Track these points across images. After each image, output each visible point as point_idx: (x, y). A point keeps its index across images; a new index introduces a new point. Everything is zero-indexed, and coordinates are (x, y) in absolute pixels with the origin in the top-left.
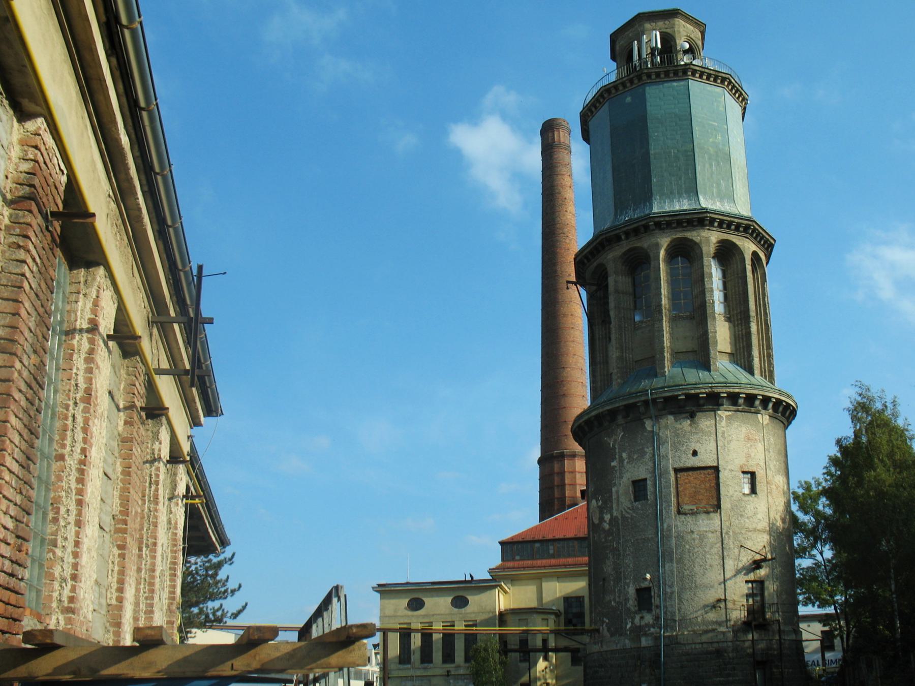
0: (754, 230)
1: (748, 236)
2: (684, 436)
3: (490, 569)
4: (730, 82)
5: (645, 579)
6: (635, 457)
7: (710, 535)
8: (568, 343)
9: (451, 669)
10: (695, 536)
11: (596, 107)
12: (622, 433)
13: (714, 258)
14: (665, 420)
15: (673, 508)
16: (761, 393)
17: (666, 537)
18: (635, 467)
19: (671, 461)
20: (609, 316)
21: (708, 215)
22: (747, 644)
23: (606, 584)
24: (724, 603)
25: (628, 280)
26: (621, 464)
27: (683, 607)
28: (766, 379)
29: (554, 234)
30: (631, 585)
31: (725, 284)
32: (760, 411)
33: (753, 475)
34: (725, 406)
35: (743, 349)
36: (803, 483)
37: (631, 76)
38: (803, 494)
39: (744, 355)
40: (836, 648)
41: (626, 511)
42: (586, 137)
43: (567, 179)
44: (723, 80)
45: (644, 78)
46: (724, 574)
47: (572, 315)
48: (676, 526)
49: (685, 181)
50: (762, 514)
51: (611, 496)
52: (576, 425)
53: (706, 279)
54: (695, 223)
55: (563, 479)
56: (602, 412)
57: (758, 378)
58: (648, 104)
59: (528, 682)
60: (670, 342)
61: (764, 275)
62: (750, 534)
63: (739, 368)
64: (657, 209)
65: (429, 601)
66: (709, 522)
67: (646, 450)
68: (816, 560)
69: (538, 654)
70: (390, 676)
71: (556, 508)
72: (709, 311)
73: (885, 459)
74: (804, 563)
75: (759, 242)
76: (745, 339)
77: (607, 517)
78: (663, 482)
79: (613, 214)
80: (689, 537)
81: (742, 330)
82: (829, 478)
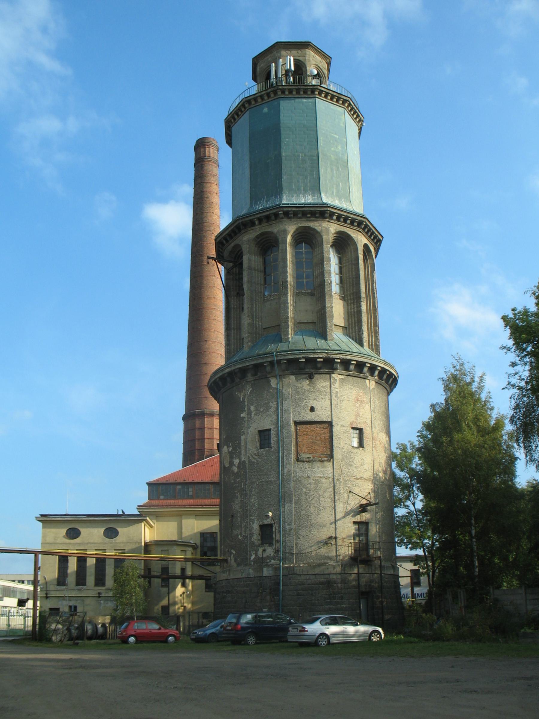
0: (366, 226)
1: (361, 230)
3: (138, 506)
4: (350, 105)
6: (261, 410)
7: (324, 481)
10: (311, 481)
11: (238, 115)
12: (251, 389)
13: (332, 246)
14: (287, 379)
15: (293, 456)
16: (369, 361)
18: (261, 419)
19: (291, 415)
20: (243, 289)
21: (329, 209)
22: (353, 576)
23: (234, 520)
24: (334, 540)
27: (299, 542)
28: (372, 350)
29: (202, 231)
31: (340, 269)
32: (368, 377)
33: (361, 430)
34: (338, 371)
35: (355, 324)
37: (269, 90)
38: (400, 453)
40: (421, 584)
41: (253, 457)
42: (229, 141)
44: (344, 102)
45: (279, 93)
47: (214, 298)
51: (240, 443)
54: (317, 215)
55: (203, 434)
56: (234, 370)
57: (366, 349)
60: (293, 314)
62: (357, 481)
63: (351, 340)
64: (286, 201)
66: (323, 469)
67: (270, 404)
68: (409, 510)
69: (177, 580)
71: (196, 458)
73: (471, 424)
74: (400, 512)
75: (370, 237)
76: (356, 316)
77: (236, 461)
78: (285, 433)
79: (249, 203)
80: (306, 482)
81: (354, 308)
82: (422, 440)
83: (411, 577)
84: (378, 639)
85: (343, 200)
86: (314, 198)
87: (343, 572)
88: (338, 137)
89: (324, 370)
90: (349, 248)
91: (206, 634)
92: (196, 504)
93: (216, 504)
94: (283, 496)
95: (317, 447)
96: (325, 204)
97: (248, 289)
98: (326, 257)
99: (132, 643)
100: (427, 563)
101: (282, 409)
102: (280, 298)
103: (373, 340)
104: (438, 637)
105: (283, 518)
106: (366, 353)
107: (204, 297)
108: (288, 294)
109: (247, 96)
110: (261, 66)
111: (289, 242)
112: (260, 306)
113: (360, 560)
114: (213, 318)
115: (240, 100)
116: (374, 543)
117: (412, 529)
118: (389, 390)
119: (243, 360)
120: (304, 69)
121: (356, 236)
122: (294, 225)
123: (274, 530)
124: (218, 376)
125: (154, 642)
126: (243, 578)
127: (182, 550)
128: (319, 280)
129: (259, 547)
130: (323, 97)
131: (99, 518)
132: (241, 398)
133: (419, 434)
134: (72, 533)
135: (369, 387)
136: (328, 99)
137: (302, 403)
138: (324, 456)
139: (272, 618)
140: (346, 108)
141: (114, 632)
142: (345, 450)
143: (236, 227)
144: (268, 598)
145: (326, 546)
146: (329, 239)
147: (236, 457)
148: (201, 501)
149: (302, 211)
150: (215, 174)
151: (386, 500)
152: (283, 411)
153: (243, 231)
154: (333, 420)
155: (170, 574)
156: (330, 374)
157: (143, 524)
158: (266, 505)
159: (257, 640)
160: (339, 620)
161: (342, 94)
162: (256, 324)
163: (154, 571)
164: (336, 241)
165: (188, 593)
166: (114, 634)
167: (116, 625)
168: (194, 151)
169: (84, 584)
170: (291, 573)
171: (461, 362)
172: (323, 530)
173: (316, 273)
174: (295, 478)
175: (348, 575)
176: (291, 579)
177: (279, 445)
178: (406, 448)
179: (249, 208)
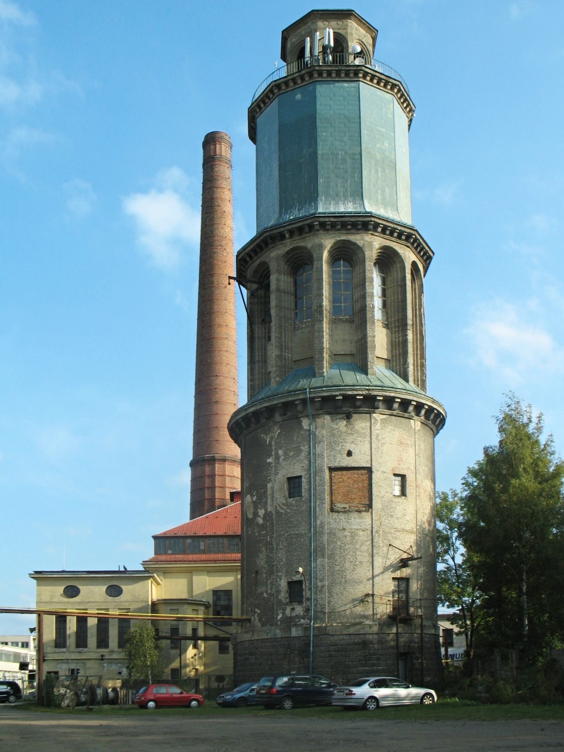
0: (416, 240)
1: (409, 245)
2: (340, 436)
3: (143, 562)
4: (399, 90)
5: (298, 572)
6: (291, 455)
7: (361, 533)
8: (221, 352)
9: (105, 654)
10: (346, 533)
11: (265, 103)
14: (322, 420)
15: (327, 506)
17: (319, 533)
18: (290, 464)
20: (270, 316)
21: (373, 219)
22: (391, 636)
24: (371, 598)
25: (290, 280)
26: (277, 462)
27: (332, 600)
28: (418, 386)
29: (212, 245)
30: (283, 578)
31: (384, 291)
32: (413, 417)
33: (403, 477)
34: (380, 410)
36: (441, 494)
37: (303, 72)
38: (440, 503)
39: (400, 361)
40: (454, 645)
41: (281, 507)
42: (253, 135)
43: (227, 192)
44: (394, 86)
45: (316, 75)
46: (373, 570)
47: (226, 326)
49: (351, 185)
50: (410, 516)
51: (266, 492)
52: (233, 421)
53: (367, 284)
54: (359, 227)
55: (213, 482)
56: (261, 408)
57: (411, 385)
58: (318, 103)
59: (179, 668)
60: (329, 343)
61: (421, 286)
62: (398, 534)
63: (394, 374)
65: (84, 589)
66: (360, 520)
67: (302, 448)
68: (448, 564)
69: (188, 641)
70: (46, 658)
71: (206, 508)
72: (369, 316)
74: (440, 567)
75: (419, 253)
76: (401, 346)
77: (261, 512)
78: (317, 480)
80: (341, 534)
81: (399, 338)
84: (431, 702)
85: (389, 208)
86: (355, 205)
87: (380, 632)
88: (384, 131)
89: (364, 409)
91: (235, 698)
92: (209, 559)
93: (230, 559)
94: (315, 550)
95: (353, 496)
96: (369, 213)
97: (276, 315)
98: (369, 277)
99: (152, 708)
100: (465, 621)
101: (315, 453)
102: (313, 326)
103: (419, 374)
106: (412, 389)
107: (214, 325)
108: (323, 320)
109: (276, 79)
110: (292, 41)
111: (325, 259)
112: (290, 335)
113: (400, 619)
114: (225, 349)
115: (268, 84)
116: (415, 600)
117: (451, 587)
118: (435, 431)
119: (271, 398)
120: (344, 45)
123: (304, 587)
124: (241, 416)
125: (175, 707)
126: (269, 639)
127: (193, 608)
128: (359, 305)
132: (268, 440)
134: (70, 590)
137: (338, 447)
138: (362, 505)
140: (394, 94)
141: (126, 696)
142: (386, 499)
143: (263, 241)
146: (372, 256)
147: (261, 507)
148: (213, 556)
149: (342, 222)
151: (429, 553)
152: (316, 456)
153: (270, 246)
155: (180, 635)
156: (370, 413)
160: (388, 682)
161: (391, 76)
162: (285, 356)
163: (163, 632)
164: (381, 258)
165: (201, 655)
166: (126, 699)
168: (202, 148)
169: (85, 646)
170: (322, 633)
171: (517, 400)
173: (357, 295)
174: (328, 530)
175: (385, 635)
177: (311, 493)
178: (447, 497)
179: (278, 217)
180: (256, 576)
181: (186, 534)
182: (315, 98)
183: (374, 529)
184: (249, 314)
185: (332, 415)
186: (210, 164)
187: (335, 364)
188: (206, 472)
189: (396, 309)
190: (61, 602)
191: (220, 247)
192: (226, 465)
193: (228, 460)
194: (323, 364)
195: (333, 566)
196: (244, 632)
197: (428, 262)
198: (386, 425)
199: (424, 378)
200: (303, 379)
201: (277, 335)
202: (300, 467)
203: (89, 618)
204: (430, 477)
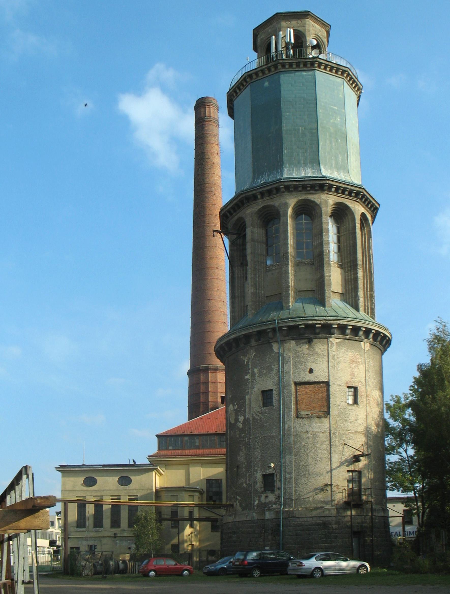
0: (364, 196)
1: (358, 200)
3: (149, 456)
4: (348, 75)
5: (270, 467)
6: (264, 372)
7: (321, 435)
8: (213, 280)
9: (117, 532)
10: (309, 435)
11: (240, 89)
13: (330, 216)
14: (288, 344)
15: (293, 413)
17: (287, 435)
19: (292, 376)
21: (328, 182)
24: (330, 487)
25: (262, 231)
27: (298, 489)
29: (204, 192)
30: (259, 471)
32: (363, 339)
33: (355, 389)
34: (335, 335)
37: (270, 65)
38: (394, 405)
39: (352, 295)
40: (414, 523)
41: (257, 415)
42: (231, 113)
43: (215, 147)
44: (343, 72)
45: (280, 67)
46: (331, 465)
47: (217, 258)
48: (295, 427)
51: (245, 402)
52: (218, 345)
54: (317, 188)
55: (207, 388)
57: (362, 314)
59: (178, 544)
60: (294, 282)
61: (370, 232)
62: (352, 435)
63: (347, 305)
65: (100, 480)
66: (320, 425)
67: (273, 367)
68: (402, 456)
69: (185, 522)
71: (201, 410)
72: (325, 259)
74: (392, 458)
75: (367, 205)
76: (353, 283)
77: (241, 418)
78: (285, 393)
79: (252, 177)
81: (351, 275)
83: (403, 518)
84: (365, 572)
89: (322, 335)
90: (346, 218)
91: (217, 568)
93: (221, 453)
94: (284, 449)
95: (315, 405)
96: (324, 177)
99: (152, 576)
100: (417, 504)
101: (284, 371)
102: (281, 268)
103: (369, 304)
104: (416, 571)
105: (284, 468)
106: (363, 318)
108: (289, 264)
110: (262, 37)
115: (242, 75)
118: (382, 350)
119: (247, 327)
120: (303, 39)
121: (353, 206)
122: (295, 198)
123: (275, 479)
125: (170, 575)
126: (248, 521)
129: (262, 493)
130: (322, 69)
131: (114, 468)
133: (411, 388)
135: (364, 349)
136: (328, 71)
139: (274, 555)
140: (345, 78)
144: (270, 537)
145: (322, 492)
146: (328, 211)
147: (241, 414)
148: (206, 450)
149: (303, 185)
150: (216, 134)
153: (246, 205)
154: (330, 380)
155: (179, 517)
156: (327, 338)
157: (154, 473)
158: (268, 457)
159: (261, 573)
161: (341, 64)
162: (259, 292)
164: (335, 211)
166: (133, 569)
167: (134, 561)
169: (101, 526)
172: (320, 479)
173: (316, 243)
176: (291, 521)
178: (400, 399)
180: (238, 470)
181: (184, 433)
182: (279, 85)
183: (331, 432)
184: (230, 259)
185: (297, 340)
186: (201, 124)
187: (299, 299)
188: (201, 380)
189: (349, 253)
190: (82, 491)
191: (210, 193)
192: (218, 373)
193: (219, 369)
194: (289, 299)
195: (299, 462)
196: (229, 515)
197: (375, 212)
198: (341, 347)
199: (373, 307)
200: (273, 311)
201: (252, 276)
202: (271, 383)
203: (104, 505)
204: (378, 388)
